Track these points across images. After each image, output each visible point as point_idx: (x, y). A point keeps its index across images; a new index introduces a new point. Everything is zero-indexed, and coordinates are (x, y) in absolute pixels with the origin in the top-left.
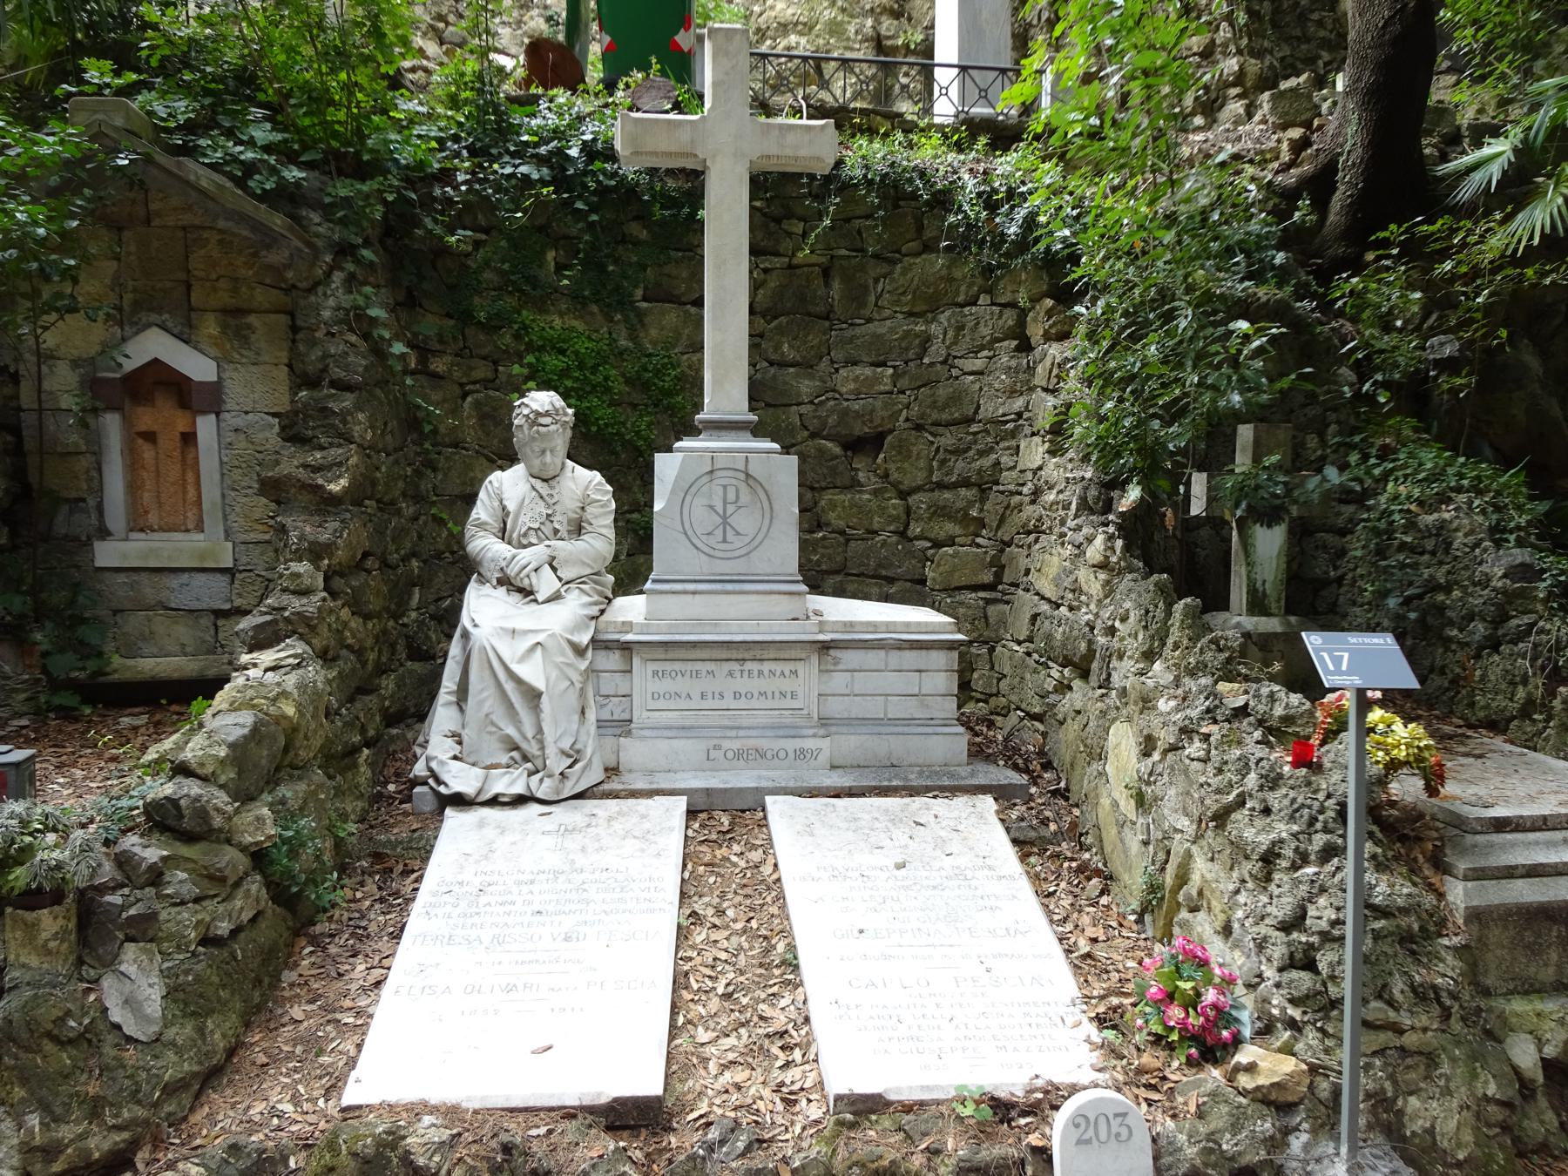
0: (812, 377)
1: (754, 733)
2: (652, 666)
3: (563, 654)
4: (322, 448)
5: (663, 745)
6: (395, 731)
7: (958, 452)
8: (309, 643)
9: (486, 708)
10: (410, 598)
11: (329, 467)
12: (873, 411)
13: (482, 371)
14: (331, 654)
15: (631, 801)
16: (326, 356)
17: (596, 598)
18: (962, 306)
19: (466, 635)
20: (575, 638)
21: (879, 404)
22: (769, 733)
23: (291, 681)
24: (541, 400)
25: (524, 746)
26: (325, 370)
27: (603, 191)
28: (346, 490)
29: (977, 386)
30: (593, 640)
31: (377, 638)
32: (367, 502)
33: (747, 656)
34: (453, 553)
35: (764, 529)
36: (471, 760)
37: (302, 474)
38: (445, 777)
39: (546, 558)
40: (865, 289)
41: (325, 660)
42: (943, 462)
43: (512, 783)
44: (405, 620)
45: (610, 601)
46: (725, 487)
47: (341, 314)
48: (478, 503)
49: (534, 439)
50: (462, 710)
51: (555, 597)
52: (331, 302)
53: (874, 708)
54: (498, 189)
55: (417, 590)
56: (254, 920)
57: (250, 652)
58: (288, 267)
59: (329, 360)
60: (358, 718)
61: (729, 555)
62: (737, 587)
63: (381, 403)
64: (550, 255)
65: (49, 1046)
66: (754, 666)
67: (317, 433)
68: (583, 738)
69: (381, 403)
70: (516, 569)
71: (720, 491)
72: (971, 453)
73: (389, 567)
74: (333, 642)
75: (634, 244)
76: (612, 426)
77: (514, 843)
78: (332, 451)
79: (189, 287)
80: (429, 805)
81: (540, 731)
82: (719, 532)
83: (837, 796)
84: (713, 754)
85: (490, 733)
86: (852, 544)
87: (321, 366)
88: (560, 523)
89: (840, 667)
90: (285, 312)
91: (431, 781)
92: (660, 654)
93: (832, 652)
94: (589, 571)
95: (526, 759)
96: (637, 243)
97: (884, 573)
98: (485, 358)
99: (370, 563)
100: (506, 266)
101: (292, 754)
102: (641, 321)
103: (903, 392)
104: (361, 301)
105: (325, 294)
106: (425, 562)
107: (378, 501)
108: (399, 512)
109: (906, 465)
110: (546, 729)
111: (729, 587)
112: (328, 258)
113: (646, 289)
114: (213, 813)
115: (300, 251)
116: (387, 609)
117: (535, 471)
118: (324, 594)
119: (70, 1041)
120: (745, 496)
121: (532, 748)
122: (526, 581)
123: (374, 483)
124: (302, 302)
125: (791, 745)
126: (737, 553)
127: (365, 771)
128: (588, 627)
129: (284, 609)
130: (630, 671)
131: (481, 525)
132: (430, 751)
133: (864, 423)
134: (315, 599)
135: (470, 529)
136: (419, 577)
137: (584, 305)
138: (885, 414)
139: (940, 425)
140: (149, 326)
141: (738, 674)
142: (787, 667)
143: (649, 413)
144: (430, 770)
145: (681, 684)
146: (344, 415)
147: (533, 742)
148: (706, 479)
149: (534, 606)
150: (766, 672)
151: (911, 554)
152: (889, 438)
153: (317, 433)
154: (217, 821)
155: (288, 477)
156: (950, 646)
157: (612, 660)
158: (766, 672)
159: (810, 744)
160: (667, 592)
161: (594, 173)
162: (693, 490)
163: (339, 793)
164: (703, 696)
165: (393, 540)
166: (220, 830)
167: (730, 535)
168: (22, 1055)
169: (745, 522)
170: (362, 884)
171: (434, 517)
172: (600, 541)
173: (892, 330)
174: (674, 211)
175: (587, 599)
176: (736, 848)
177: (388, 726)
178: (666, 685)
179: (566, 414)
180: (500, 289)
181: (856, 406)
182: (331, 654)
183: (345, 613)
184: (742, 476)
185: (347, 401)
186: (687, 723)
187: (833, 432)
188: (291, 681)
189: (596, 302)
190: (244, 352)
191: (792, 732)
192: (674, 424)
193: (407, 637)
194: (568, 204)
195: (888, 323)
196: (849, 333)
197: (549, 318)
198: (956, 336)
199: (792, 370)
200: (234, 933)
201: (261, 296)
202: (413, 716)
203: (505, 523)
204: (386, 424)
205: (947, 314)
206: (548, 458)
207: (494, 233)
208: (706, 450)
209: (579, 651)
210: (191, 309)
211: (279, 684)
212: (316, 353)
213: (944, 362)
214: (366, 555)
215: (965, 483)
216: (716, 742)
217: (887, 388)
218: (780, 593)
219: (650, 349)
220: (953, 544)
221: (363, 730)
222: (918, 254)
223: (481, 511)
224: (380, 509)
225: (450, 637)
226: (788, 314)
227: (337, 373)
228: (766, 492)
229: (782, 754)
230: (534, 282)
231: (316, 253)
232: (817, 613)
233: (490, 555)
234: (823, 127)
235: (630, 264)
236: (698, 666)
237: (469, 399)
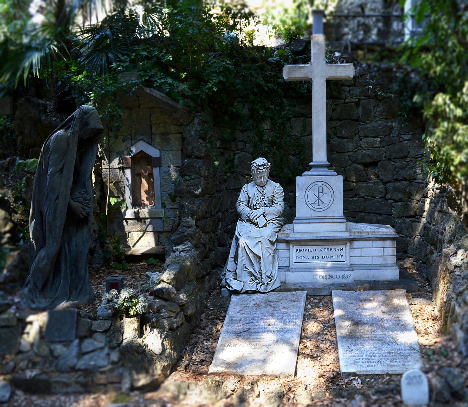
0: (353, 142)
2: (296, 248)
6: (214, 271)
7: (402, 168)
8: (191, 243)
10: (218, 226)
14: (198, 246)
17: (278, 225)
20: (271, 240)
23: (188, 255)
24: (260, 161)
25: (255, 274)
28: (200, 193)
29: (408, 145)
30: (277, 240)
32: (206, 195)
35: (332, 201)
38: (231, 285)
39: (262, 213)
41: (196, 248)
44: (217, 233)
45: (282, 226)
46: (319, 187)
50: (236, 264)
51: (265, 225)
53: (368, 261)
55: (220, 223)
56: (181, 325)
57: (175, 246)
65: (136, 354)
68: (274, 272)
70: (253, 217)
72: (407, 169)
79: (151, 127)
80: (226, 294)
86: (367, 201)
87: (191, 151)
88: (266, 200)
90: (180, 133)
91: (227, 286)
92: (297, 243)
95: (256, 278)
97: (378, 212)
101: (188, 277)
103: (383, 147)
106: (223, 213)
114: (171, 293)
118: (195, 227)
119: (141, 353)
121: (258, 276)
129: (184, 232)
130: (289, 250)
132: (226, 277)
139: (396, 158)
140: (140, 140)
144: (226, 282)
154: (173, 296)
156: (393, 239)
157: (282, 246)
158: (333, 249)
162: (309, 189)
163: (200, 290)
165: (213, 207)
166: (173, 298)
168: (130, 355)
169: (326, 199)
172: (279, 206)
177: (213, 269)
178: (301, 254)
179: (268, 165)
183: (201, 232)
187: (360, 162)
188: (188, 255)
190: (167, 147)
193: (218, 239)
196: (364, 126)
199: (346, 140)
200: (177, 327)
201: (173, 128)
209: (272, 243)
210: (152, 134)
211: (185, 256)
213: (398, 136)
215: (405, 179)
220: (401, 201)
221: (206, 270)
223: (242, 197)
225: (232, 238)
226: (344, 120)
234: (349, 65)
237: (236, 156)
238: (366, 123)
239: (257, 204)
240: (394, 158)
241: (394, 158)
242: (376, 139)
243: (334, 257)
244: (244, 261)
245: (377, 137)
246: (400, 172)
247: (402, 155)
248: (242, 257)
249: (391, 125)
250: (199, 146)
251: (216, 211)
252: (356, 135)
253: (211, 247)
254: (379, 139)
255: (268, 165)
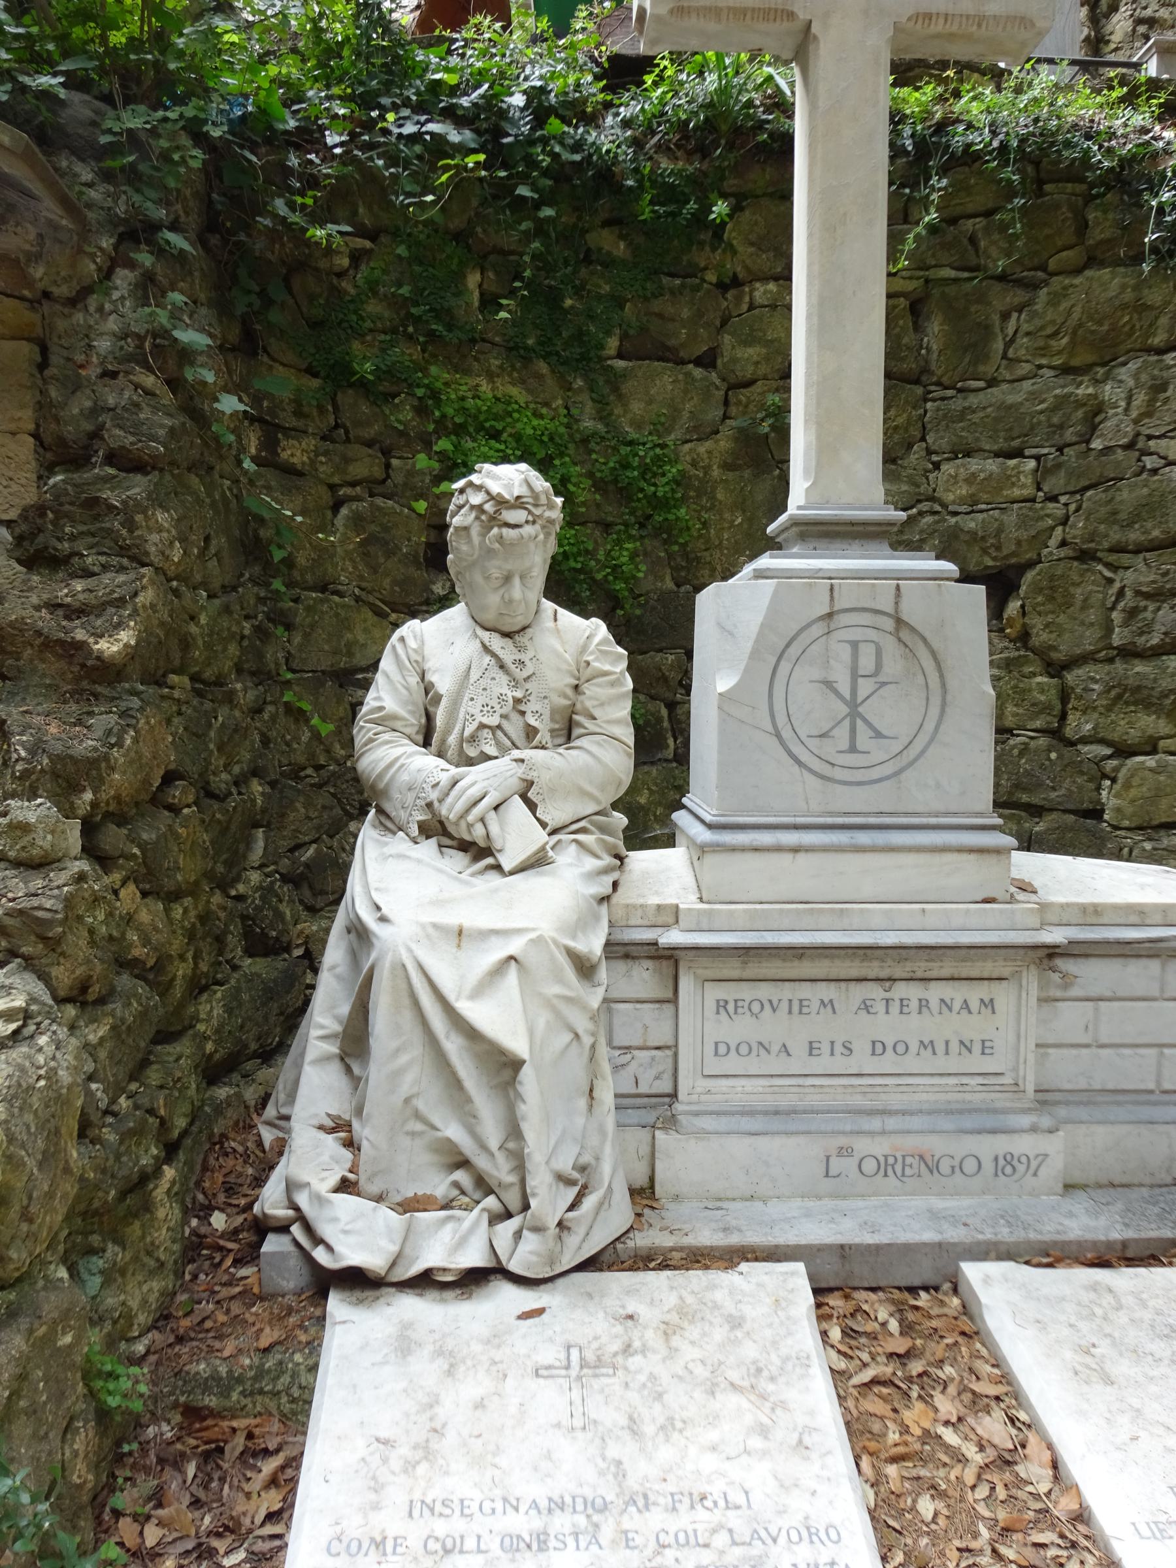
1: (916, 1122)
2: (715, 992)
3: (560, 980)
4: (87, 574)
5: (740, 1147)
8: (43, 977)
9: (406, 1087)
11: (101, 608)
12: (1000, 531)
13: (365, 465)
14: (93, 993)
15: (696, 1278)
16: (97, 409)
18: (1161, 352)
19: (359, 934)
20: (580, 946)
21: (1010, 519)
22: (946, 1123)
25: (482, 1162)
26: (96, 434)
27: (560, 173)
28: (131, 654)
31: (191, 935)
32: (174, 678)
33: (898, 972)
34: (318, 768)
35: (930, 726)
36: (374, 1188)
37: (45, 621)
38: (326, 1230)
39: (515, 784)
40: (986, 331)
42: (1132, 613)
43: (461, 1243)
44: (241, 888)
46: (855, 645)
47: (130, 345)
48: (379, 677)
49: (490, 552)
50: (356, 1082)
51: (537, 862)
52: (112, 324)
54: (393, 159)
55: (260, 833)
58: (36, 257)
59: (105, 418)
60: (151, 1112)
61: (859, 776)
62: (880, 838)
63: (199, 501)
64: (473, 280)
66: (912, 992)
67: (81, 546)
69: (199, 501)
70: (460, 806)
71: (845, 652)
73: (210, 795)
74: (99, 968)
75: (605, 265)
76: (575, 556)
77: (480, 1405)
78: (106, 578)
80: (291, 1279)
81: (514, 1131)
82: (842, 733)
83: (1102, 1263)
84: (836, 1165)
85: (413, 1134)
87: (88, 427)
88: (539, 717)
89: (1075, 992)
91: (296, 1229)
92: (731, 968)
93: (1059, 962)
94: (591, 808)
95: (484, 1186)
96: (609, 263)
97: (1025, 798)
98: (369, 444)
99: (178, 793)
100: (405, 290)
102: (616, 389)
103: (1054, 498)
104: (163, 317)
105: (100, 309)
106: (273, 784)
107: (194, 678)
108: (230, 698)
109: (1062, 618)
110: (529, 1131)
111: (863, 838)
112: (106, 243)
113: (624, 337)
115: (56, 227)
116: (209, 875)
117: (489, 617)
118: (83, 865)
120: (893, 665)
121: (500, 1170)
122: (478, 832)
123: (186, 644)
124: (61, 325)
125: (989, 1147)
126: (875, 773)
127: (166, 1212)
128: (597, 918)
130: (674, 1000)
131: (386, 721)
133: (985, 551)
134: (60, 878)
135: (363, 730)
136: (264, 811)
137: (527, 360)
138: (1024, 535)
141: (880, 1007)
142: (975, 994)
143: (631, 538)
145: (773, 1027)
146: (128, 513)
147: (500, 1157)
148: (817, 630)
149: (494, 879)
150: (934, 1004)
151: (1076, 767)
152: (1030, 576)
153: (81, 546)
155: (19, 626)
158: (934, 1004)
159: (1024, 1145)
160: (743, 849)
161: (544, 141)
162: (794, 651)
164: (812, 1049)
165: (220, 749)
167: (862, 733)
170: (158, 1498)
171: (289, 708)
173: (1034, 397)
174: (671, 208)
175: (591, 863)
176: (946, 1406)
178: (742, 1028)
179: (551, 506)
180: (394, 331)
181: (971, 524)
182: (93, 993)
183: (129, 892)
184: (889, 624)
185: (138, 487)
186: (784, 1102)
189: (545, 357)
191: (990, 1122)
192: (671, 556)
193: (244, 918)
194: (503, 190)
195: (1027, 385)
196: (958, 404)
197: (472, 382)
198: (1151, 402)
202: (255, 1056)
203: (429, 718)
204: (207, 539)
205: (1133, 366)
206: (517, 591)
207: (384, 239)
208: (815, 574)
209: (584, 968)
212: (81, 403)
213: (1130, 446)
214: (169, 778)
216: (843, 1141)
217: (1027, 492)
218: (960, 850)
219: (633, 435)
220: (1153, 751)
222: (1078, 271)
224: (199, 694)
227: (117, 437)
228: (934, 654)
229: (970, 1166)
230: (445, 315)
231: (85, 231)
232: (1025, 887)
233: (404, 777)
235: (599, 297)
236: (805, 991)
237: (344, 511)
238: (960, 391)
239: (486, 733)
240: (1112, 550)
241: (1112, 550)
242: (1012, 463)
243: (941, 1048)
244: (409, 1077)
245: (1018, 453)
246: (1148, 615)
247: (1156, 533)
248: (398, 1051)
249: (1095, 396)
250: (137, 405)
251: (236, 769)
252: (910, 446)
253: (204, 967)
254: (1032, 464)
255: (551, 506)
